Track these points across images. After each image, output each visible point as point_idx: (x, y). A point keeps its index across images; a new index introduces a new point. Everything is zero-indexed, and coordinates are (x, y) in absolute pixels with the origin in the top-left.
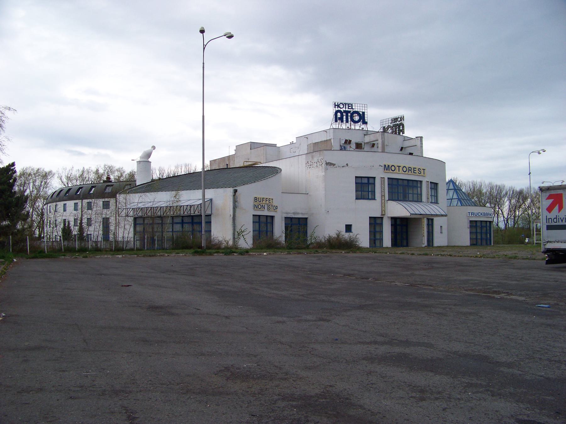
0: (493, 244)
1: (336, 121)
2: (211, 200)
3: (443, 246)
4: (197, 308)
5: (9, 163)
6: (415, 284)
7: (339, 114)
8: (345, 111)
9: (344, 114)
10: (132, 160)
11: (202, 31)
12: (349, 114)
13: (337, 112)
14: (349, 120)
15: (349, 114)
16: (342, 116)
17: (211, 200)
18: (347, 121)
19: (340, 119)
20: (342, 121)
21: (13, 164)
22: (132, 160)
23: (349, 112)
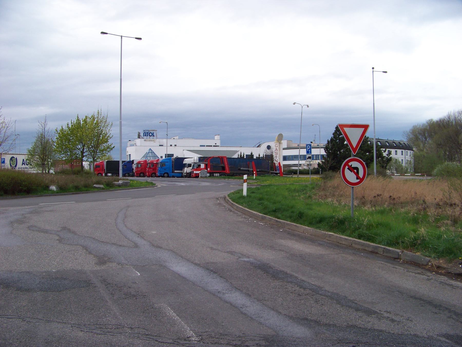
0: (124, 175)
1: (144, 136)
2: (130, 155)
3: (54, 196)
4: (395, 269)
5: (331, 138)
6: (221, 161)
7: (145, 134)
8: (147, 133)
9: (147, 134)
10: (140, 39)
11: (373, 68)
12: (148, 134)
13: (144, 133)
14: (148, 135)
15: (148, 134)
16: (146, 134)
17: (130, 155)
18: (148, 136)
19: (145, 135)
20: (146, 136)
21: (328, 140)
22: (140, 39)
23: (148, 133)
